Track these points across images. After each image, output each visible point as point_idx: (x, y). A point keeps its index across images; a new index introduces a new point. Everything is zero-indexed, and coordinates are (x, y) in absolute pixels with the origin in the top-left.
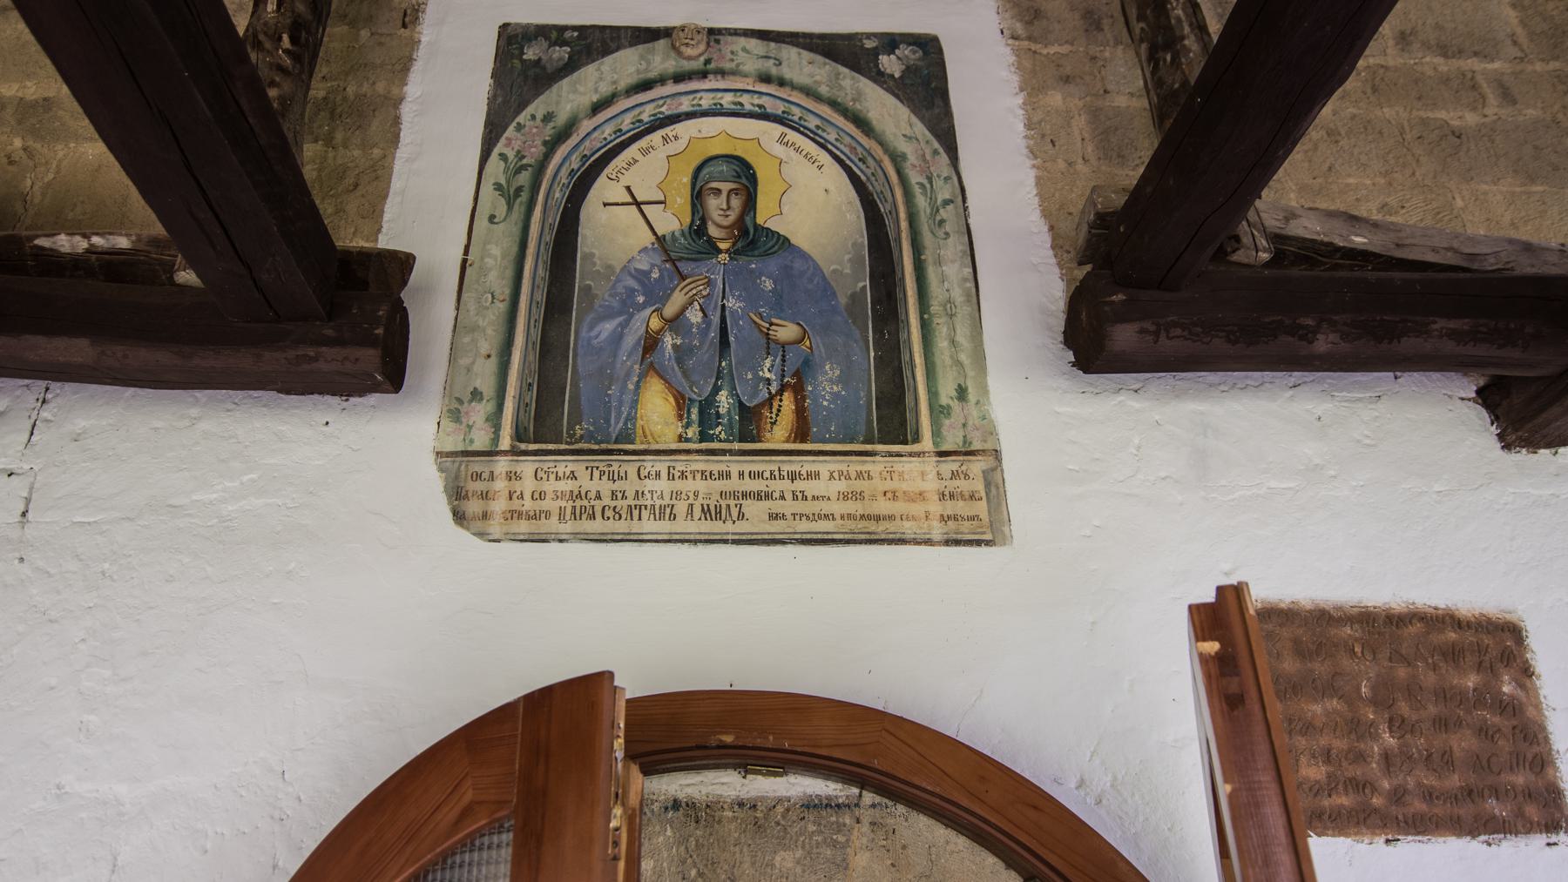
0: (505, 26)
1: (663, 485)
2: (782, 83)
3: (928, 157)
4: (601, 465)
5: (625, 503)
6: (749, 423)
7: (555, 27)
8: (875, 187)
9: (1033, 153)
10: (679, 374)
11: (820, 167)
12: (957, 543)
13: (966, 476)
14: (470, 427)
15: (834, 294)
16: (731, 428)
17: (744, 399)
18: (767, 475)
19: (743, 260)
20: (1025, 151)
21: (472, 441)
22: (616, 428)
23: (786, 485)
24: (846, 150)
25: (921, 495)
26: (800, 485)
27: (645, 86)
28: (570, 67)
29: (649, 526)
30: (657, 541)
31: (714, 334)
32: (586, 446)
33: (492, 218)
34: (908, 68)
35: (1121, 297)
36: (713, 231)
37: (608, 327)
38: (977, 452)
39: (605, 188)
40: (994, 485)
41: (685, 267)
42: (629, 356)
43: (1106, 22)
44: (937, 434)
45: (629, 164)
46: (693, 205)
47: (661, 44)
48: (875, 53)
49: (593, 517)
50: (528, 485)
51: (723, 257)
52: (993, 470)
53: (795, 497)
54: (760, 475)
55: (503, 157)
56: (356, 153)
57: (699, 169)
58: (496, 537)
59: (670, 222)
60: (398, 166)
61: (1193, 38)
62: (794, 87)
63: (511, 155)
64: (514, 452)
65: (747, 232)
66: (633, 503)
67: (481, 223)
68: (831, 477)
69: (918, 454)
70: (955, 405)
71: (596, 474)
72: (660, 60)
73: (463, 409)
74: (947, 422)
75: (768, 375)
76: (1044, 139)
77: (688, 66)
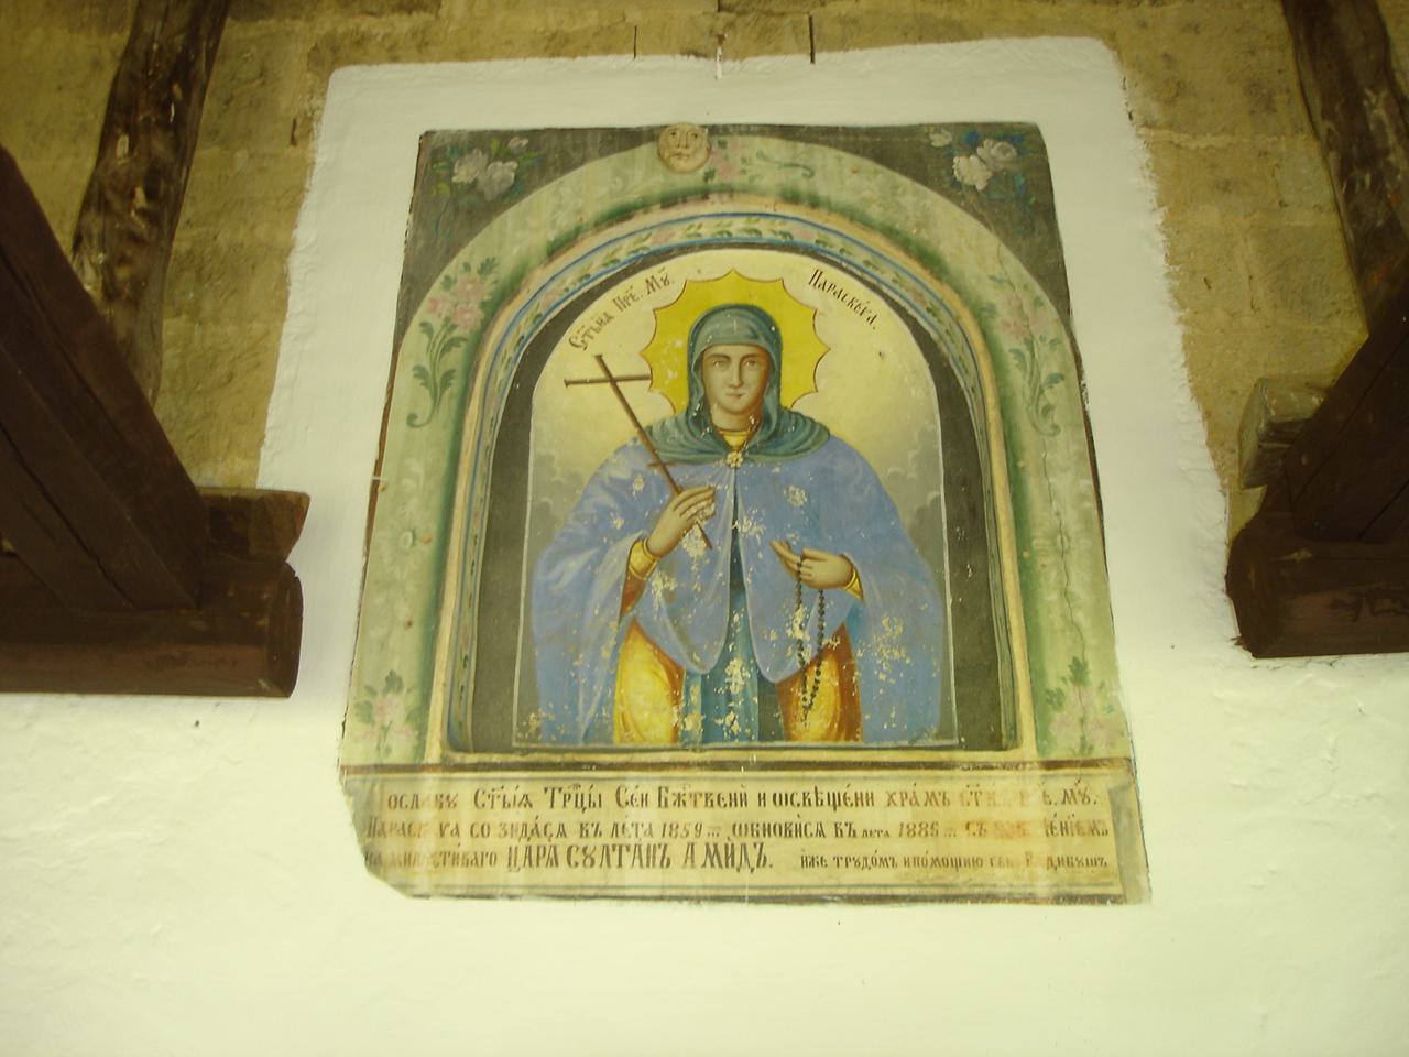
0: (428, 135)
1: (651, 815)
2: (815, 203)
3: (1027, 310)
4: (566, 786)
5: (600, 842)
6: (774, 707)
7: (497, 134)
8: (951, 350)
9: (1179, 299)
10: (674, 636)
11: (871, 320)
12: (1072, 899)
13: (1085, 798)
14: (385, 730)
15: (893, 510)
16: (748, 715)
17: (766, 672)
18: (798, 799)
19: (762, 461)
20: (1167, 297)
21: (388, 750)
22: (584, 719)
23: (824, 814)
24: (909, 296)
25: (1020, 829)
26: (846, 814)
27: (622, 214)
28: (516, 191)
29: (633, 875)
30: (643, 898)
31: (722, 573)
32: (544, 757)
33: (412, 418)
34: (996, 175)
35: (1305, 554)
36: (719, 419)
37: (573, 565)
38: (1101, 761)
39: (566, 359)
40: (1125, 812)
41: (680, 474)
42: (602, 610)
43: (1280, 99)
44: (1042, 734)
45: (601, 323)
46: (691, 381)
47: (645, 151)
48: (947, 155)
49: (554, 862)
50: (465, 815)
51: (732, 456)
52: (1124, 788)
53: (838, 833)
54: (788, 799)
55: (426, 327)
56: (231, 329)
57: (699, 327)
58: (424, 890)
59: (658, 406)
60: (285, 348)
61: (1400, 150)
62: (832, 209)
63: (437, 324)
64: (446, 766)
65: (766, 420)
66: (610, 841)
67: (398, 427)
68: (891, 802)
69: (1016, 766)
70: (1070, 690)
71: (559, 798)
72: (640, 174)
73: (377, 701)
74: (1057, 716)
75: (799, 635)
76: (1194, 278)
77: (681, 182)
